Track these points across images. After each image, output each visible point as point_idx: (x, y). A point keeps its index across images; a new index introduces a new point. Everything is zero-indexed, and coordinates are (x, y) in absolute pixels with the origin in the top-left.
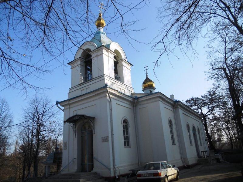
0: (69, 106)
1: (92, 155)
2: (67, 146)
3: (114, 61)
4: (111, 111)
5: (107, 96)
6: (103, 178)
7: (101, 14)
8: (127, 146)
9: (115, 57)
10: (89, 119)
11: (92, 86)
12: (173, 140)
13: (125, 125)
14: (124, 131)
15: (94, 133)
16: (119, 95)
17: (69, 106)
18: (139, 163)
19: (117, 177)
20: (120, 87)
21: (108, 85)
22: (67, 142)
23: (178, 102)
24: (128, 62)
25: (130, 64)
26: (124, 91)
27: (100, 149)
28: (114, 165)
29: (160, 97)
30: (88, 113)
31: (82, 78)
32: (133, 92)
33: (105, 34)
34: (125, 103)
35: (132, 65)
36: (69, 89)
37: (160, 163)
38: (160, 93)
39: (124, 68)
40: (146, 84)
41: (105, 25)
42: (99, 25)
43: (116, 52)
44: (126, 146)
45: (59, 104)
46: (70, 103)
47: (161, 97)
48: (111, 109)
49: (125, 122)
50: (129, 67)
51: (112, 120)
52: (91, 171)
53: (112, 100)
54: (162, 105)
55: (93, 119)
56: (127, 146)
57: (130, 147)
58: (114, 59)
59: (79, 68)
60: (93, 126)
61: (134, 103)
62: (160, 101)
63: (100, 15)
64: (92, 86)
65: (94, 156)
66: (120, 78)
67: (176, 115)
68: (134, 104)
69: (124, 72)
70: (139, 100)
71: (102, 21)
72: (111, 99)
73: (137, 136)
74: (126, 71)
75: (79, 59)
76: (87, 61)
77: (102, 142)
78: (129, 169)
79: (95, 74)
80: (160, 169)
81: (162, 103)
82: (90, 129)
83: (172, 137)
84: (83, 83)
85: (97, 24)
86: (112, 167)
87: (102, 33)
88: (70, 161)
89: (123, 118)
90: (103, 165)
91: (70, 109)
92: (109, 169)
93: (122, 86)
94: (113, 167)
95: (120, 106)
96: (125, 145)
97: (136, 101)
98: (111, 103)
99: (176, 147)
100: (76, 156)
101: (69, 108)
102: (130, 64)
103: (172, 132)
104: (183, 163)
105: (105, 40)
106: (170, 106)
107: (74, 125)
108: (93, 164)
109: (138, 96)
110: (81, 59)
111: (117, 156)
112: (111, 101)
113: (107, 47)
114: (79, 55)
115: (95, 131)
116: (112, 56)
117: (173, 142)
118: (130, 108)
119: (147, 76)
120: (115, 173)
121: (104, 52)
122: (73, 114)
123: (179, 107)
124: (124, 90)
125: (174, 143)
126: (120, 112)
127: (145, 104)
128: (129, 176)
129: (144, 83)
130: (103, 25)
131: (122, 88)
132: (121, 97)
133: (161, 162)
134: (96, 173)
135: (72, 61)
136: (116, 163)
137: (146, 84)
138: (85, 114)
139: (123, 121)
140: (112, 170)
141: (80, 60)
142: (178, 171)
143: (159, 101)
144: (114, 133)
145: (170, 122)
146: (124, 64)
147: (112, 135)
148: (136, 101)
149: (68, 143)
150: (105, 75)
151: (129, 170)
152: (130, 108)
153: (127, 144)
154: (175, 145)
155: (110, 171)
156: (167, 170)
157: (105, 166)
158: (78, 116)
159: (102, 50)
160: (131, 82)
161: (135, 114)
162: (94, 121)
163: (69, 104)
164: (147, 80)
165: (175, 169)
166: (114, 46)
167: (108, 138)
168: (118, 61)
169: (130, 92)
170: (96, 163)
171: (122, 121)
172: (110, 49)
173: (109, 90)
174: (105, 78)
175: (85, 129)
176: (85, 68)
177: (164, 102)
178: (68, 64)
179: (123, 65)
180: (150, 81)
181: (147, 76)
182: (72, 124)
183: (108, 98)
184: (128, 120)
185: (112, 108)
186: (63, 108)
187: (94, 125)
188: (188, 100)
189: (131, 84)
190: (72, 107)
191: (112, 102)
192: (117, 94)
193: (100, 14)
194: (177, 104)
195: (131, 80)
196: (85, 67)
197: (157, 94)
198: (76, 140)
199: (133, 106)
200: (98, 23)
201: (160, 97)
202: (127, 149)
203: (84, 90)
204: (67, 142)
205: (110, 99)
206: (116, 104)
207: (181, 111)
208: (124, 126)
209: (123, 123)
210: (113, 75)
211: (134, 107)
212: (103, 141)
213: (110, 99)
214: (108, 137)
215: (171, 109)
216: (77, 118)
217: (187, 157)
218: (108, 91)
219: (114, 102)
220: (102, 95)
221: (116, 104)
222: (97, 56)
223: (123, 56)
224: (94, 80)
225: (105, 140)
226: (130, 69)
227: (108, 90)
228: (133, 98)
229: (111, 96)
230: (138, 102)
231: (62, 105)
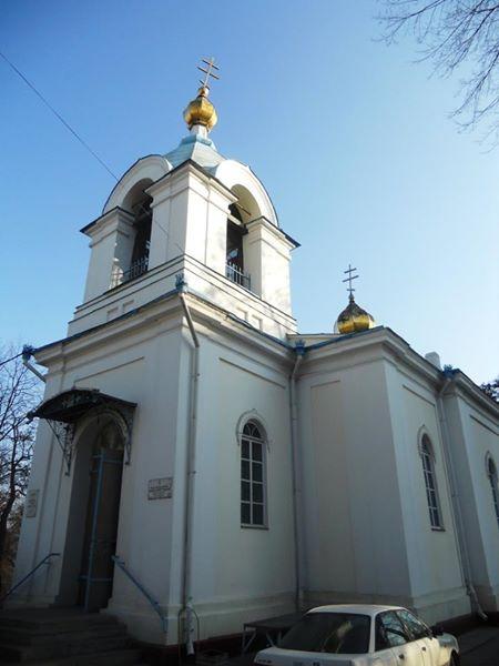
0: (65, 363)
1: (114, 546)
2: (36, 507)
3: (230, 225)
4: (196, 380)
5: (182, 325)
6: (133, 644)
7: (207, 91)
8: (255, 522)
9: (234, 209)
10: (118, 411)
11: (144, 293)
12: (435, 512)
14: (245, 465)
15: (128, 463)
16: (241, 332)
17: (65, 363)
18: (298, 592)
19: (191, 651)
20: (246, 308)
21: (186, 284)
22: (38, 491)
23: (452, 373)
24: (281, 231)
25: (287, 237)
26: (257, 322)
27: (143, 530)
28: (185, 598)
29: (385, 345)
30: (109, 387)
31: (118, 274)
32: (294, 330)
33: (213, 145)
34: (263, 365)
35: (297, 245)
37: (369, 618)
38: (389, 329)
39: (264, 247)
40: (348, 324)
41: (214, 120)
42: (197, 120)
43: (239, 191)
44: (249, 522)
45: (32, 358)
46: (66, 352)
47: (395, 349)
48: (194, 376)
49: (253, 429)
50: (285, 248)
51: (194, 417)
52: (102, 611)
53: (200, 343)
54: (394, 378)
55: (127, 409)
56: (255, 522)
57: (267, 529)
59: (112, 242)
60: (126, 435)
62: (387, 360)
63: (203, 92)
64: (144, 293)
65: (120, 550)
66: (249, 280)
67: (447, 421)
68: (292, 370)
69: (264, 261)
70: (310, 359)
71: (206, 108)
72: (198, 336)
73: (297, 488)
74: (272, 260)
75: (114, 215)
76: (139, 220)
77: (150, 499)
78: (248, 622)
79: (154, 260)
80: (367, 651)
81: (394, 369)
82: (120, 448)
83: (433, 499)
84: (120, 286)
85: (188, 117)
86: (174, 603)
87: (203, 142)
88: (39, 561)
89: (242, 416)
90: (142, 590)
92: (162, 612)
93: (252, 303)
94: (179, 605)
95: (238, 370)
96: (245, 518)
97: (300, 357)
98: (197, 353)
99: (448, 539)
100: (60, 547)
101: (64, 371)
102: (287, 237)
103: (430, 480)
104: (472, 602)
105: (203, 154)
106: (426, 385)
107: (67, 429)
108: (112, 582)
109: (308, 344)
110: (121, 215)
111: (200, 552)
112: (197, 346)
114: (119, 200)
115: (132, 456)
116: (225, 204)
117: (436, 518)
118: (270, 381)
119: (351, 298)
120: (184, 629)
121: (194, 181)
122: (62, 387)
123: (457, 390)
124: (260, 320)
125: (438, 525)
126: (228, 393)
127: (327, 372)
128: (245, 649)
129: (342, 319)
130: (207, 119)
131: (251, 312)
132: (242, 338)
133: (374, 611)
134: (113, 620)
135: (94, 222)
136: (192, 592)
137: (348, 324)
138: (97, 388)
139: (241, 430)
140: (172, 617)
141: (117, 216)
142: (453, 652)
143: (387, 360)
144: (198, 464)
145: (426, 443)
146: (265, 234)
147: (190, 472)
148: (300, 357)
149: (41, 492)
150: (186, 257)
151: (246, 625)
152: (270, 381)
153: (253, 514)
154: (443, 530)
155: (164, 621)
156: (402, 657)
157: (148, 597)
159: (188, 176)
160: (289, 299)
161: (294, 408)
162: (132, 418)
163: (65, 358)
164: (353, 309)
165: (444, 645)
166: (233, 173)
167: (171, 485)
168: (248, 226)
169: (282, 328)
170: (120, 580)
171: (238, 426)
172: (216, 176)
173: (189, 302)
174: (186, 264)
175: (105, 443)
177: (403, 369)
178: (83, 231)
179: (263, 237)
180: (362, 313)
181: (351, 298)
182: (60, 427)
183: (186, 332)
184: (263, 423)
185: (200, 372)
186: (43, 370)
187: (130, 433)
188: (486, 384)
189: (286, 299)
190: (72, 369)
191: (201, 348)
192: (226, 323)
193: (202, 88)
194: (449, 380)
195: (288, 290)
196: (133, 243)
197: (377, 333)
198: (68, 484)
199: (290, 378)
200: (192, 115)
201: (385, 345)
202: (252, 535)
203: (117, 308)
204: (38, 491)
205: (195, 339)
206: (221, 359)
207: (464, 409)
208: (245, 445)
209: (245, 432)
211: (293, 381)
212: (151, 495)
213: (195, 339)
214: (171, 479)
215: (428, 395)
216: (70, 404)
217: (488, 581)
218: (184, 306)
219: (210, 353)
220: (169, 324)
221: (221, 359)
222: (171, 198)
223: (264, 208)
225: (67, 474)
226: (290, 258)
227: (187, 303)
228: (290, 348)
229: (196, 325)
230: (306, 365)
231: (43, 359)
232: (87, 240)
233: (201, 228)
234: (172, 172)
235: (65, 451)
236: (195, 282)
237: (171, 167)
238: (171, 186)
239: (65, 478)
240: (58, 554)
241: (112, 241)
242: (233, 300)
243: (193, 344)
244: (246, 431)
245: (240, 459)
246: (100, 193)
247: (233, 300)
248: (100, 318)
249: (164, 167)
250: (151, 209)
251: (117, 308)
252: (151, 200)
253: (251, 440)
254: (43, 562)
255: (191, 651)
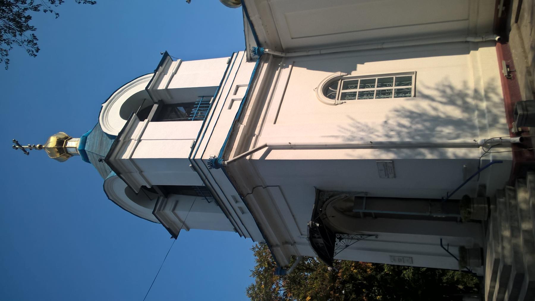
3: (157, 118)
8: (410, 84)
9: (142, 117)
11: (226, 189)
13: (342, 91)
14: (362, 95)
19: (517, 139)
25: (161, 64)
36: (243, 237)
58: (146, 120)
59: (182, 213)
60: (343, 196)
61: (274, 56)
64: (226, 189)
74: (189, 75)
77: (395, 177)
91: (295, 243)
100: (436, 239)
102: (161, 64)
107: (340, 239)
110: (159, 209)
112: (266, 146)
113: (119, 141)
114: (147, 212)
131: (231, 97)
135: (169, 230)
145: (230, 108)
158: (315, 237)
166: (113, 122)
174: (198, 157)
176: (185, 196)
187: (343, 192)
198: (383, 236)
204: (391, 256)
206: (275, 123)
208: (344, 97)
210: (189, 128)
216: (321, 241)
218: (234, 160)
221: (275, 123)
223: (140, 86)
224: (211, 184)
225: (377, 236)
226: (179, 60)
227: (231, 158)
232: (183, 232)
233: (163, 142)
234: (118, 174)
235: (358, 239)
236: (212, 150)
237: (113, 173)
238: (131, 172)
239: (380, 238)
240: (441, 240)
241: (185, 211)
242: (223, 117)
243: (266, 148)
244: (332, 97)
245: (356, 100)
246: (143, 227)
247: (223, 117)
248: (248, 218)
249: (112, 179)
250: (152, 187)
251: (240, 208)
252: (144, 187)
253: (340, 90)
254: (447, 251)
255: (517, 139)
